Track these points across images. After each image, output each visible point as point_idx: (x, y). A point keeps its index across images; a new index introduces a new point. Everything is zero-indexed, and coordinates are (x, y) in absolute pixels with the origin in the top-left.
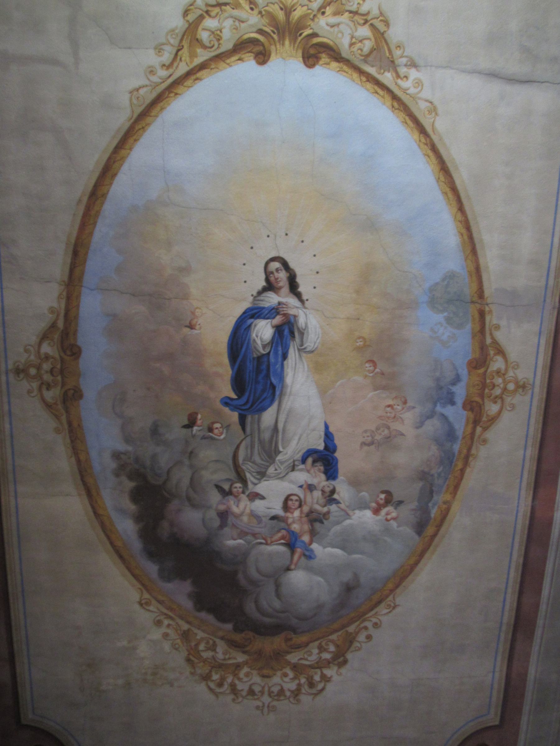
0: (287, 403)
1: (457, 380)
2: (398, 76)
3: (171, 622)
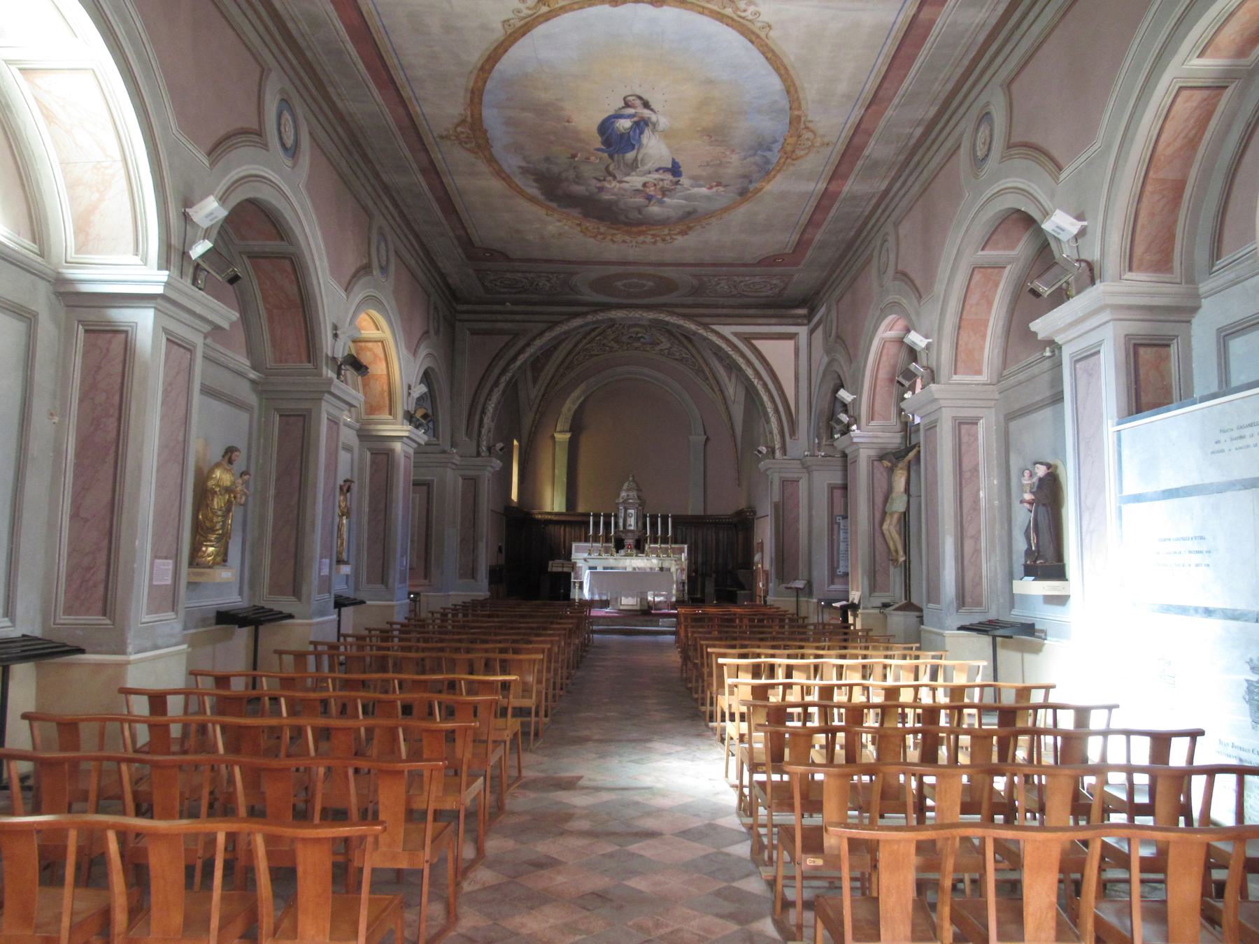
0: (643, 151)
1: (775, 141)
2: (738, 9)
3: (743, 14)
